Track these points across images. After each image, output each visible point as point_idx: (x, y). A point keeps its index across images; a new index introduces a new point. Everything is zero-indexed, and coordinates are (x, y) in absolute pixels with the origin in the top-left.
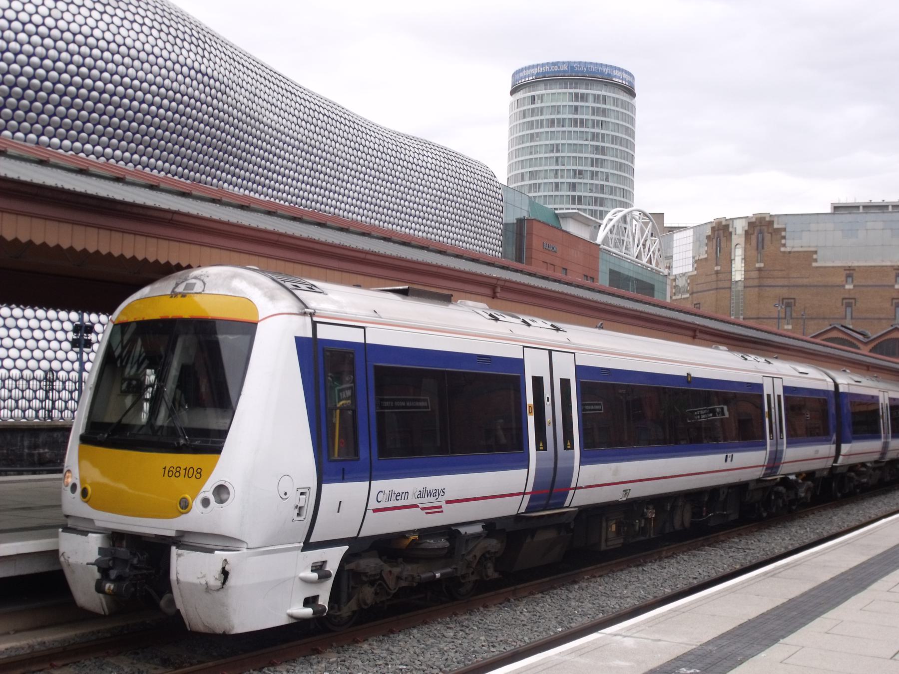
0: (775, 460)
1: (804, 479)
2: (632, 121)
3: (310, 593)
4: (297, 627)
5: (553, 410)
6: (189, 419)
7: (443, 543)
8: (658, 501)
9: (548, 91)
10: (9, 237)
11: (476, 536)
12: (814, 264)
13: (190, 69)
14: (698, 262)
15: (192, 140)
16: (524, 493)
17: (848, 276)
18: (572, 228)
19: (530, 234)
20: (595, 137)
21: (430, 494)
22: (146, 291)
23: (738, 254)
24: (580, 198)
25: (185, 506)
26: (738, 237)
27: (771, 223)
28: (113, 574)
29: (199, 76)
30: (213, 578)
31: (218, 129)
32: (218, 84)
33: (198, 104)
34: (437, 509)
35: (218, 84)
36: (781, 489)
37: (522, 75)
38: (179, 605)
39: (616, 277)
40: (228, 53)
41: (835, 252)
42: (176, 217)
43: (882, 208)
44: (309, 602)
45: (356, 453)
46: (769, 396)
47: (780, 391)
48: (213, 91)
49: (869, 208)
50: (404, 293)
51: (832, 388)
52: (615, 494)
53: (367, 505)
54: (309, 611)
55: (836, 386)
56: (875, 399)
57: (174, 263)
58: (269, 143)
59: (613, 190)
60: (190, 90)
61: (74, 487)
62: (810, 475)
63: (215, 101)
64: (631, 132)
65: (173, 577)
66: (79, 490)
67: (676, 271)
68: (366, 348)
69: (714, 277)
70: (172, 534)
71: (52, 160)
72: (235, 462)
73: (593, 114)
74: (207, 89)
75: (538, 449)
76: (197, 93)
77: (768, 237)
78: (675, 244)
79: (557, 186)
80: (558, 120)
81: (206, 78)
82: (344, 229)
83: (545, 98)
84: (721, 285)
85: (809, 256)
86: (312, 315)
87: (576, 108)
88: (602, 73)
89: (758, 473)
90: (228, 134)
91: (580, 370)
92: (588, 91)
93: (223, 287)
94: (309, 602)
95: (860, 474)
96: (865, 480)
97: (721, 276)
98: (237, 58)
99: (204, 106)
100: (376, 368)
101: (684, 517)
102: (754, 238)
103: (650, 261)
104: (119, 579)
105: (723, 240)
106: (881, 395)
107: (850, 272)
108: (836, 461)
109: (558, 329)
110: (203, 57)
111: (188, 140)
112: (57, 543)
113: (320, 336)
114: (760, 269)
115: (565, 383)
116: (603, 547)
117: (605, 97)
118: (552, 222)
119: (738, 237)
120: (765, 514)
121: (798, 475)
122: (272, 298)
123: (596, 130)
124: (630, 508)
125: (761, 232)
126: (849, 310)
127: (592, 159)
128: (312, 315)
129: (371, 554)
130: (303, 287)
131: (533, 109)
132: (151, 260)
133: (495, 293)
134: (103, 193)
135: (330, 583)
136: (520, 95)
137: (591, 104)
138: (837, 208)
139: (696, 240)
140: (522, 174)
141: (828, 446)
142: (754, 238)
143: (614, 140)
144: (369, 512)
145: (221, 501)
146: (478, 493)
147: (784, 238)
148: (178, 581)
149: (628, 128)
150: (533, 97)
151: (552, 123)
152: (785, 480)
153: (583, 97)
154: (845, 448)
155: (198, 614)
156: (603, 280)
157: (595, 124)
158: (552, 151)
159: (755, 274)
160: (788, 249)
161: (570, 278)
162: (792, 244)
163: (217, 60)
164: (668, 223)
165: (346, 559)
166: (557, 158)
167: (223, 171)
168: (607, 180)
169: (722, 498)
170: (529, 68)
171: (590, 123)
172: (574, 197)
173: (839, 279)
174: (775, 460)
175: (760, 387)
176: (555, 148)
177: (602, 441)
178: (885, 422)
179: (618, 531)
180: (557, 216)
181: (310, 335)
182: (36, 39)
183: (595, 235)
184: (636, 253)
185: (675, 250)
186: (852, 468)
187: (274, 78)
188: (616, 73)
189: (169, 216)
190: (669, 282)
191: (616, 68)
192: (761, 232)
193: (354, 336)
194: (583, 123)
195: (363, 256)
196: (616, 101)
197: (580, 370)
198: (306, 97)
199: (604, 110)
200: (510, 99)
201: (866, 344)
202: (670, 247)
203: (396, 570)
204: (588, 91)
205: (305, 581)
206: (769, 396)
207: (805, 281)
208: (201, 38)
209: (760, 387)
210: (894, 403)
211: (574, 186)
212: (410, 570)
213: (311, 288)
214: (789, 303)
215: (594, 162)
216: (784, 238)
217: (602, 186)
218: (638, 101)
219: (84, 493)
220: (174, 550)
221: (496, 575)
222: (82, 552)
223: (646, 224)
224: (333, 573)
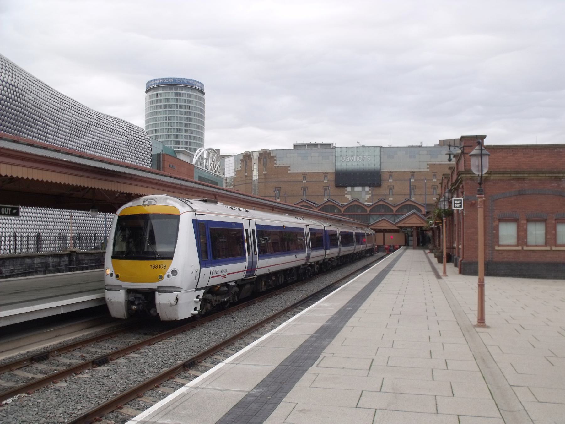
2: (203, 106)
4: (194, 316)
7: (226, 289)
9: (164, 92)
10: (3, 175)
11: (234, 286)
12: (289, 172)
13: (6, 83)
14: (237, 172)
15: (8, 118)
17: (304, 177)
18: (182, 157)
19: (164, 160)
20: (186, 113)
22: (130, 204)
23: (255, 167)
24: (179, 142)
25: (161, 278)
27: (270, 153)
29: (11, 86)
30: (173, 301)
31: (21, 113)
32: (20, 90)
33: (11, 100)
34: (224, 277)
35: (20, 90)
37: (151, 83)
38: (158, 312)
39: (200, 178)
40: (23, 75)
41: (299, 166)
42: (133, 176)
43: (316, 145)
44: (196, 309)
45: (207, 258)
46: (247, 230)
47: (309, 231)
48: (18, 94)
49: (310, 145)
50: (205, 201)
54: (197, 312)
56: (352, 233)
58: (44, 119)
59: (195, 138)
60: (13, 96)
62: (317, 262)
63: (19, 99)
64: (202, 111)
65: (157, 302)
66: (114, 275)
67: (226, 176)
68: (207, 222)
69: (244, 178)
72: (177, 263)
73: (185, 102)
74: (15, 93)
76: (10, 95)
77: (268, 160)
78: (226, 163)
79: (169, 136)
80: (169, 105)
81: (14, 88)
82: (128, 167)
83: (162, 95)
84: (248, 181)
85: (287, 168)
86: (195, 211)
87: (177, 99)
88: (189, 83)
89: (303, 262)
90: (25, 115)
91: (257, 226)
92: (183, 92)
93: (160, 202)
95: (332, 262)
97: (248, 178)
98: (28, 78)
99: (14, 101)
100: (211, 229)
101: (282, 280)
102: (262, 160)
105: (248, 161)
106: (305, 227)
107: (305, 175)
110: (9, 75)
111: (6, 118)
112: (104, 295)
114: (265, 175)
115: (253, 230)
116: (261, 291)
117: (191, 95)
118: (173, 155)
121: (314, 262)
122: (183, 206)
123: (187, 110)
125: (265, 158)
126: (305, 192)
127: (185, 124)
128: (195, 211)
131: (157, 100)
134: (96, 165)
136: (150, 93)
137: (184, 98)
138: (296, 146)
139: (236, 161)
140: (152, 131)
142: (262, 160)
143: (195, 115)
147: (276, 160)
148: (159, 303)
149: (201, 109)
150: (157, 94)
151: (166, 106)
152: (311, 265)
153: (181, 95)
154: (328, 251)
155: (165, 314)
157: (186, 107)
158: (166, 120)
159: (263, 177)
160: (278, 165)
163: (19, 79)
164: (221, 153)
166: (169, 123)
167: (23, 133)
168: (192, 133)
170: (155, 80)
171: (184, 107)
172: (177, 141)
173: (300, 178)
175: (241, 225)
176: (168, 118)
177: (264, 252)
178: (339, 241)
179: (265, 284)
180: (175, 152)
183: (192, 160)
184: (210, 168)
185: (226, 166)
186: (330, 259)
187: (45, 88)
188: (195, 83)
189: (130, 176)
190: (224, 181)
191: (195, 81)
192: (265, 158)
194: (180, 106)
196: (196, 97)
197: (257, 226)
198: (61, 97)
199: (190, 101)
201: (317, 207)
202: (224, 165)
203: (215, 298)
204: (183, 92)
205: (196, 302)
206: (247, 230)
207: (285, 180)
209: (241, 225)
210: (313, 232)
211: (176, 136)
212: (218, 298)
214: (278, 189)
215: (186, 125)
216: (276, 160)
217: (190, 136)
218: (206, 97)
219: (117, 276)
220: (157, 293)
222: (117, 299)
223: (214, 155)
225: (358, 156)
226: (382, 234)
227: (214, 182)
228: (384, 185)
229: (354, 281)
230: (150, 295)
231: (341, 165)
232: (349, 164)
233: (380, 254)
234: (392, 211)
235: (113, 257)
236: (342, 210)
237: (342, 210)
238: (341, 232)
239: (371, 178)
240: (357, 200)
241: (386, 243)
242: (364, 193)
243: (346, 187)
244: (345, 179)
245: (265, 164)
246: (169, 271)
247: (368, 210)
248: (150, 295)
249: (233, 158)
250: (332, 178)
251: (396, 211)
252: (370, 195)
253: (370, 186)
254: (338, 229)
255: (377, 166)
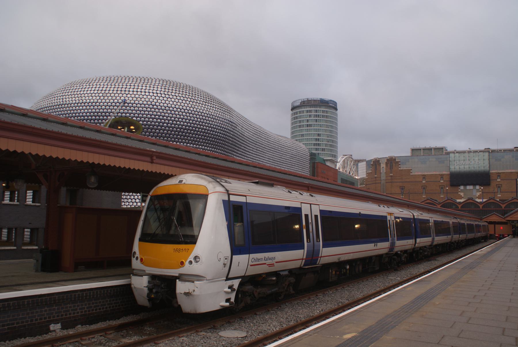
0: (393, 245)
1: (404, 253)
3: (228, 297)
5: (312, 227)
6: (181, 231)
8: (350, 262)
10: (4, 149)
11: (286, 276)
14: (368, 174)
16: (303, 259)
17: (424, 178)
18: (328, 164)
21: (270, 259)
25: (182, 263)
26: (383, 165)
27: (395, 159)
28: (154, 290)
36: (395, 257)
39: (343, 180)
41: (419, 169)
43: (430, 149)
44: (228, 300)
46: (306, 216)
51: (412, 217)
52: (335, 259)
53: (243, 263)
54: (228, 304)
55: (414, 216)
56: (428, 221)
57: (170, 174)
61: (137, 258)
62: (405, 251)
66: (139, 259)
70: (177, 275)
71: (145, 140)
75: (307, 242)
77: (394, 164)
84: (377, 182)
85: (409, 171)
91: (321, 211)
93: (191, 181)
94: (228, 300)
96: (426, 253)
97: (377, 179)
102: (389, 165)
103: (350, 173)
104: (157, 292)
107: (424, 177)
108: (415, 244)
109: (312, 196)
113: (231, 199)
114: (391, 176)
115: (316, 216)
116: (330, 280)
118: (323, 163)
119: (383, 165)
120: (389, 267)
121: (401, 251)
124: (339, 265)
129: (249, 281)
130: (223, 181)
132: (150, 171)
133: (152, 160)
135: (234, 294)
136: (294, 111)
141: (412, 240)
144: (249, 266)
145: (197, 262)
146: (289, 258)
152: (396, 254)
154: (418, 240)
155: (187, 306)
156: (339, 182)
161: (329, 181)
162: (403, 167)
165: (241, 285)
169: (373, 261)
174: (393, 245)
181: (227, 199)
182: (188, 114)
183: (336, 165)
186: (420, 248)
193: (242, 199)
195: (216, 167)
197: (321, 211)
200: (291, 112)
201: (439, 204)
205: (227, 293)
206: (306, 216)
207: (408, 180)
208: (229, 110)
213: (226, 182)
214: (402, 188)
219: (142, 260)
220: (178, 282)
221: (293, 292)
222: (140, 284)
224: (236, 289)
225: (469, 160)
226: (493, 225)
227: (349, 182)
228: (493, 184)
229: (381, 299)
230: (170, 282)
231: (455, 168)
232: (462, 167)
233: (492, 241)
234: (501, 207)
235: (140, 240)
236: (460, 206)
237: (460, 206)
238: (453, 222)
239: (481, 179)
240: (471, 199)
241: (496, 233)
242: (475, 191)
243: (460, 186)
244: (459, 179)
245: (391, 168)
246: (191, 258)
247: (481, 206)
248: (170, 282)
249: (365, 163)
250: (447, 178)
251: (505, 207)
252: (481, 193)
253: (480, 185)
254: (451, 221)
255: (487, 168)
